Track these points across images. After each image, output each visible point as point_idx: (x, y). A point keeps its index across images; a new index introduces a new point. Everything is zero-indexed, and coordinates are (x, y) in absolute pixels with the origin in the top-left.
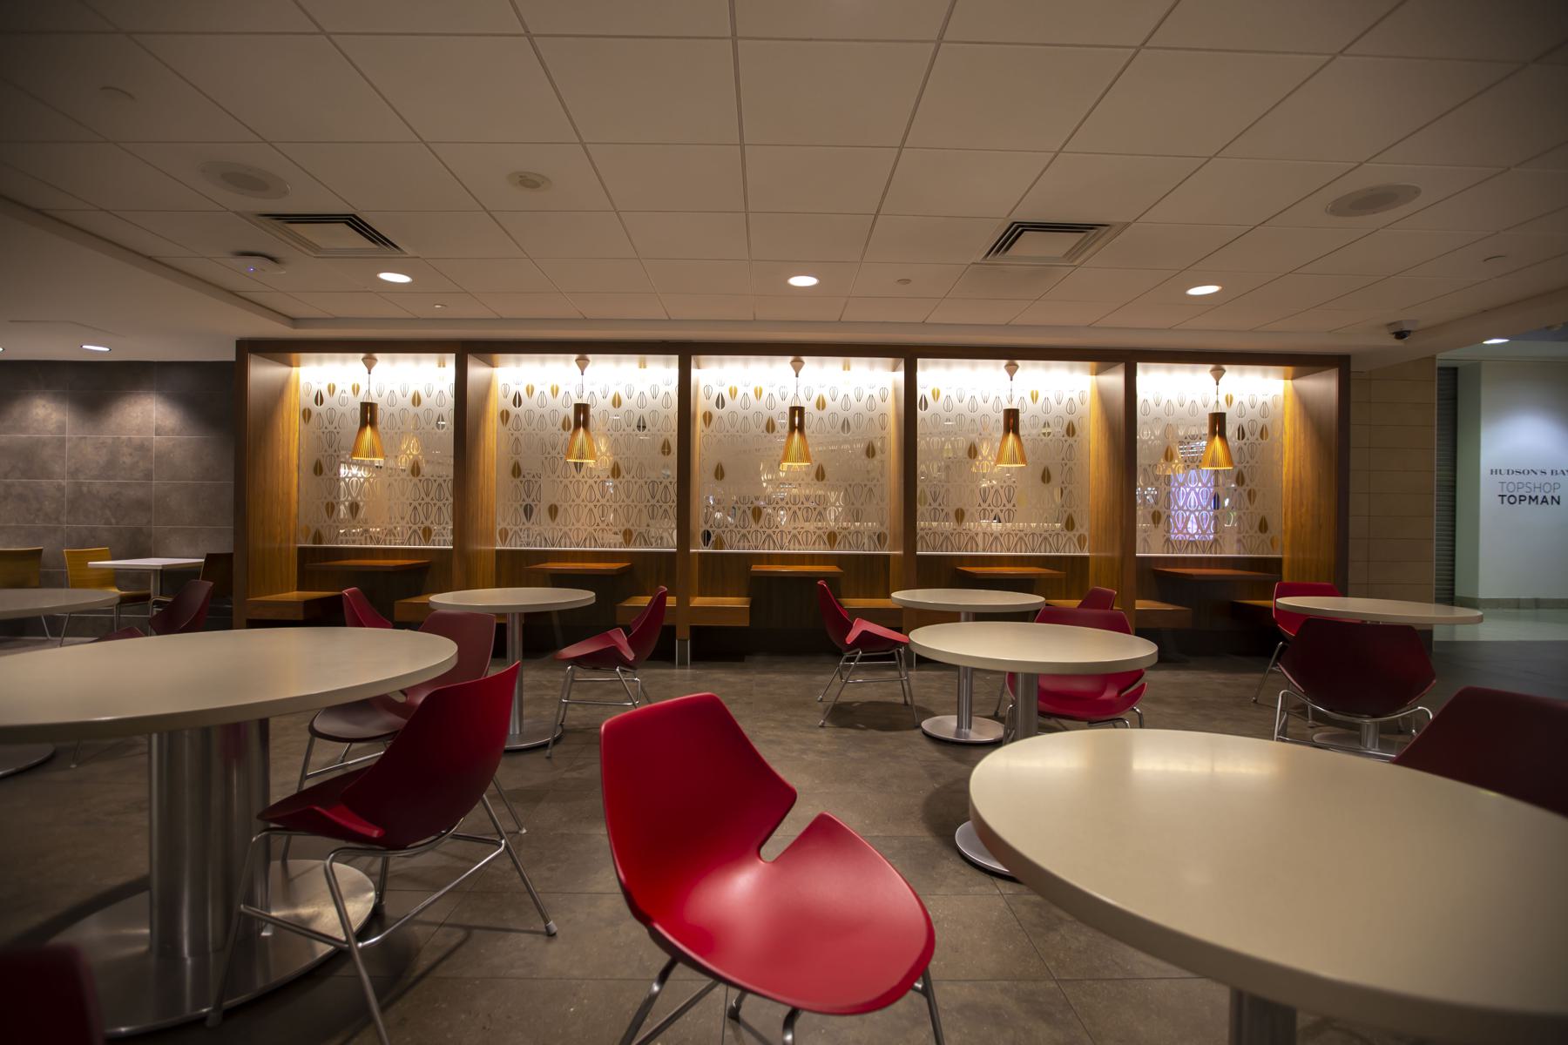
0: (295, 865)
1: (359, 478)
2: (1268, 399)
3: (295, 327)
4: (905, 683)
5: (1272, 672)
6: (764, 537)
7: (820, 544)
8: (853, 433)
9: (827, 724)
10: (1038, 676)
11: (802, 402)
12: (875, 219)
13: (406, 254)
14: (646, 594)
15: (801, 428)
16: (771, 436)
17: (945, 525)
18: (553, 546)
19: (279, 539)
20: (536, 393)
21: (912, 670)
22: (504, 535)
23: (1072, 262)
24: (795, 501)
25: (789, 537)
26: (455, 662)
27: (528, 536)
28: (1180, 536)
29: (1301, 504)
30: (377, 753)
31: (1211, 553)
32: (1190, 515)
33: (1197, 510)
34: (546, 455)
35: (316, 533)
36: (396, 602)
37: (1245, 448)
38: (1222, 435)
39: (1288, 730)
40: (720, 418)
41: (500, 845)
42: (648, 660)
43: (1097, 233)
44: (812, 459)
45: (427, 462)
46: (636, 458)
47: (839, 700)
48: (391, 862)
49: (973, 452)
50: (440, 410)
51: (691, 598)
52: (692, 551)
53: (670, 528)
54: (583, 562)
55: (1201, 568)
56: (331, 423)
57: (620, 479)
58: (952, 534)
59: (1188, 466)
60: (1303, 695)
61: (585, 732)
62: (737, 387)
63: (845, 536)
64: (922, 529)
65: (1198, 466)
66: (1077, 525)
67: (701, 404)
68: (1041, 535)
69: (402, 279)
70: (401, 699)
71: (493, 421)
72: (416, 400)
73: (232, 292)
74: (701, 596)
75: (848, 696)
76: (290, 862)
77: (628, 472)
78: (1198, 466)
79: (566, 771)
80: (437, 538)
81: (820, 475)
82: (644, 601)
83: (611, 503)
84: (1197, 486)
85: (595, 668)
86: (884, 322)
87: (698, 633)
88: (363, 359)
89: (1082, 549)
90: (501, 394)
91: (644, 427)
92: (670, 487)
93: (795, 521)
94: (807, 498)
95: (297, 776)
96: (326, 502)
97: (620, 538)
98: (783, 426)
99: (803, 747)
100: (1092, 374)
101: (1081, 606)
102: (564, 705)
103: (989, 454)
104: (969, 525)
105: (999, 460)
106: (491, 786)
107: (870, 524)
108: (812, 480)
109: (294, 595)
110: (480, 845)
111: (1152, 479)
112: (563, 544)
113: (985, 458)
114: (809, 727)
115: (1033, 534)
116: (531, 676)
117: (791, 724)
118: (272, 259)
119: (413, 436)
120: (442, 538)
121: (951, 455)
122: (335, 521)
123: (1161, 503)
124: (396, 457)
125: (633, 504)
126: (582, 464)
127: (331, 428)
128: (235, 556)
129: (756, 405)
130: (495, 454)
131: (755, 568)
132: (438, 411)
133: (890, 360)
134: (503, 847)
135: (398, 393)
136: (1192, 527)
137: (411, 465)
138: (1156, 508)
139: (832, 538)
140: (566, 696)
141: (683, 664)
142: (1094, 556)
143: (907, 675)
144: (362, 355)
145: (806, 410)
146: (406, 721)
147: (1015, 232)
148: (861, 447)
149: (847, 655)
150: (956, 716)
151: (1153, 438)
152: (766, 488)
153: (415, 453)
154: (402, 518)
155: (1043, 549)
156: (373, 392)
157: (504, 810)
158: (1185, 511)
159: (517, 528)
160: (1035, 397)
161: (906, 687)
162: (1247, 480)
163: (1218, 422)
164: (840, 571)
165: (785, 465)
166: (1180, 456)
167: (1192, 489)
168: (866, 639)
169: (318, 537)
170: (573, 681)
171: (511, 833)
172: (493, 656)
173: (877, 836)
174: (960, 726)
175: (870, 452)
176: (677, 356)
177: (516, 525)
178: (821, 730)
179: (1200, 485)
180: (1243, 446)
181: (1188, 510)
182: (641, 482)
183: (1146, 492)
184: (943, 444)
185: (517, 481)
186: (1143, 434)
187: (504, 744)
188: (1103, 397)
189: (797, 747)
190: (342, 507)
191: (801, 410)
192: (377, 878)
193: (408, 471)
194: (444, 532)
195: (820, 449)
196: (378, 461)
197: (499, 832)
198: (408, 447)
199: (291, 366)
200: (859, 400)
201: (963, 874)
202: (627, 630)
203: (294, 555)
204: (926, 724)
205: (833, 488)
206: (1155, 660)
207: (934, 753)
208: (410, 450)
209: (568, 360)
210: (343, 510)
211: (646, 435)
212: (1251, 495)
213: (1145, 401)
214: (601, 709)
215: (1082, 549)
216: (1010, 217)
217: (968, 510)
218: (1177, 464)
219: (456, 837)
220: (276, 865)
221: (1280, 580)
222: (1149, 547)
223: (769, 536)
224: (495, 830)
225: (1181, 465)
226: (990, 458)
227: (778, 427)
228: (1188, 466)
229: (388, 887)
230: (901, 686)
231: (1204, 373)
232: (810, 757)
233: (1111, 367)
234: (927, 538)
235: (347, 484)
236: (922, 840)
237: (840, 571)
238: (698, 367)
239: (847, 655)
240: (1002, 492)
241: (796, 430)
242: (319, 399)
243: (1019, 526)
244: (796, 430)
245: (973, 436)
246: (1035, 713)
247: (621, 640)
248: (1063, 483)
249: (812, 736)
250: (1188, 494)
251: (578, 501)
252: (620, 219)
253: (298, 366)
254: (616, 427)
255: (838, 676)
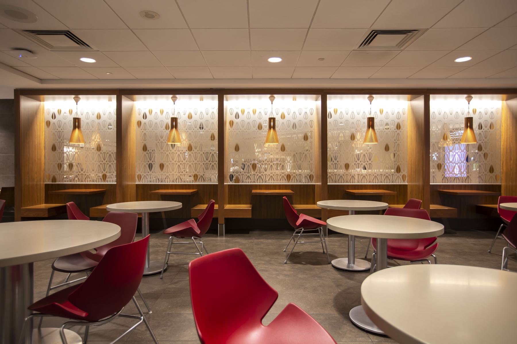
0: (44, 330)
1: (73, 152)
2: (494, 110)
3: (42, 83)
4: (323, 243)
5: (497, 238)
6: (257, 177)
7: (283, 180)
8: (298, 129)
9: (288, 262)
10: (387, 239)
11: (274, 116)
12: (308, 30)
13: (93, 49)
14: (204, 204)
15: (274, 127)
16: (260, 131)
17: (340, 171)
18: (162, 182)
19: (36, 180)
20: (153, 113)
21: (326, 237)
22: (140, 177)
23: (400, 48)
24: (271, 161)
25: (269, 177)
26: (120, 235)
27: (150, 178)
28: (451, 175)
29: (511, 159)
30: (84, 278)
31: (466, 183)
32: (455, 165)
33: (459, 163)
34: (158, 141)
35: (53, 178)
36: (91, 208)
37: (482, 134)
38: (471, 127)
39: (508, 266)
40: (237, 123)
41: (141, 319)
42: (206, 233)
43: (412, 34)
44: (279, 141)
45: (104, 145)
46: (199, 142)
47: (293, 251)
48: (90, 328)
49: (353, 137)
50: (109, 121)
51: (225, 205)
52: (225, 184)
53: (215, 173)
54: (175, 189)
55: (461, 190)
56: (59, 127)
57: (192, 151)
58: (344, 175)
59: (454, 142)
60: (515, 249)
61: (179, 268)
62: (245, 109)
63: (294, 177)
64: (330, 173)
65: (459, 142)
66: (402, 170)
67: (228, 117)
68: (385, 175)
69: (91, 61)
70: (94, 252)
71: (134, 126)
72: (99, 117)
73: (11, 67)
74: (229, 204)
75: (297, 249)
76: (43, 329)
77: (196, 148)
78: (459, 142)
79: (169, 285)
80: (109, 179)
81: (283, 148)
82: (204, 207)
83: (108, 162)
84: (459, 152)
85: (182, 237)
86: (312, 78)
87: (228, 221)
88: (74, 98)
89: (404, 181)
90: (137, 114)
91: (203, 128)
92: (215, 155)
93: (271, 170)
94: (277, 159)
95: (45, 289)
96: (148, 163)
97: (192, 178)
98: (266, 127)
99: (277, 273)
100: (408, 101)
101: (405, 207)
102: (168, 254)
103: (361, 138)
104: (352, 171)
105: (365, 141)
106: (137, 292)
107: (306, 171)
108: (279, 151)
109: (43, 206)
110: (130, 319)
111: (437, 149)
112: (166, 181)
113: (358, 140)
114: (280, 263)
115: (381, 175)
116: (153, 241)
117: (272, 262)
118: (30, 51)
119: (97, 133)
120: (111, 179)
121: (343, 139)
122: (62, 172)
123: (442, 160)
124: (90, 142)
125: (198, 163)
126: (174, 145)
127: (59, 129)
128: (15, 188)
129: (253, 117)
130: (135, 142)
131: (254, 191)
132: (109, 121)
133: (314, 96)
134: (142, 320)
135: (90, 113)
136: (456, 171)
137: (97, 146)
138: (439, 162)
139: (289, 177)
140: (169, 250)
141: (221, 235)
142: (409, 185)
143: (324, 239)
144: (73, 96)
145: (276, 119)
146: (97, 263)
147: (373, 35)
148: (301, 136)
149: (297, 230)
150: (347, 258)
151: (437, 129)
152: (258, 155)
153: (98, 140)
154: (93, 170)
155: (397, 182)
156: (79, 113)
157: (142, 303)
158: (453, 163)
159: (145, 174)
160: (381, 112)
161: (324, 245)
162: (483, 149)
163: (469, 121)
164: (293, 192)
165: (267, 145)
166: (451, 138)
167: (457, 153)
168: (305, 223)
169: (54, 179)
170: (172, 243)
171: (145, 313)
172: (136, 233)
173: (313, 314)
174: (349, 263)
175: (306, 138)
176: (217, 95)
177: (145, 173)
178: (286, 265)
179: (460, 151)
180: (481, 133)
181: (455, 163)
182: (202, 153)
183: (434, 156)
184: (339, 134)
185: (145, 153)
186: (433, 128)
187: (143, 271)
188: (414, 111)
189: (275, 272)
190: (65, 166)
191: (274, 119)
192: (83, 336)
193: (96, 149)
194: (112, 176)
195: (283, 137)
196: (82, 144)
197: (140, 313)
198: (95, 138)
199: (40, 101)
200: (300, 114)
201: (354, 332)
202: (197, 220)
203: (43, 187)
204: (333, 262)
205: (289, 155)
206: (443, 233)
207: (337, 275)
208: (96, 139)
209: (167, 98)
210: (66, 167)
211: (204, 132)
212: (485, 155)
213: (434, 112)
214: (185, 256)
215: (404, 181)
216: (371, 28)
217: (165, 164)
218: (449, 142)
219: (120, 316)
220: (35, 331)
221: (500, 195)
222: (436, 180)
223: (260, 176)
224: (138, 312)
225: (451, 142)
226: (361, 140)
227: (263, 127)
228: (454, 142)
229: (88, 340)
230: (321, 245)
231: (462, 99)
232: (281, 277)
233: (418, 97)
234: (332, 177)
235: (67, 155)
236: (334, 316)
237: (293, 192)
238: (227, 100)
239: (297, 230)
240: (366, 155)
241: (272, 129)
242: (54, 116)
243: (374, 171)
244: (272, 129)
245: (353, 130)
246: (386, 257)
247: (194, 225)
248: (395, 151)
249: (281, 267)
250: (455, 155)
251: (173, 162)
252: (192, 33)
253: (44, 101)
254: (190, 128)
255: (293, 240)
